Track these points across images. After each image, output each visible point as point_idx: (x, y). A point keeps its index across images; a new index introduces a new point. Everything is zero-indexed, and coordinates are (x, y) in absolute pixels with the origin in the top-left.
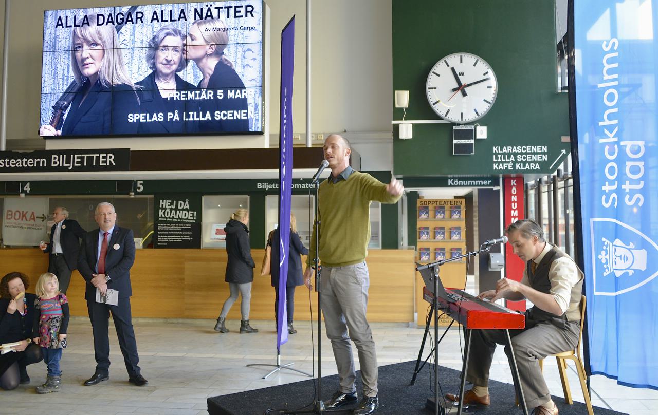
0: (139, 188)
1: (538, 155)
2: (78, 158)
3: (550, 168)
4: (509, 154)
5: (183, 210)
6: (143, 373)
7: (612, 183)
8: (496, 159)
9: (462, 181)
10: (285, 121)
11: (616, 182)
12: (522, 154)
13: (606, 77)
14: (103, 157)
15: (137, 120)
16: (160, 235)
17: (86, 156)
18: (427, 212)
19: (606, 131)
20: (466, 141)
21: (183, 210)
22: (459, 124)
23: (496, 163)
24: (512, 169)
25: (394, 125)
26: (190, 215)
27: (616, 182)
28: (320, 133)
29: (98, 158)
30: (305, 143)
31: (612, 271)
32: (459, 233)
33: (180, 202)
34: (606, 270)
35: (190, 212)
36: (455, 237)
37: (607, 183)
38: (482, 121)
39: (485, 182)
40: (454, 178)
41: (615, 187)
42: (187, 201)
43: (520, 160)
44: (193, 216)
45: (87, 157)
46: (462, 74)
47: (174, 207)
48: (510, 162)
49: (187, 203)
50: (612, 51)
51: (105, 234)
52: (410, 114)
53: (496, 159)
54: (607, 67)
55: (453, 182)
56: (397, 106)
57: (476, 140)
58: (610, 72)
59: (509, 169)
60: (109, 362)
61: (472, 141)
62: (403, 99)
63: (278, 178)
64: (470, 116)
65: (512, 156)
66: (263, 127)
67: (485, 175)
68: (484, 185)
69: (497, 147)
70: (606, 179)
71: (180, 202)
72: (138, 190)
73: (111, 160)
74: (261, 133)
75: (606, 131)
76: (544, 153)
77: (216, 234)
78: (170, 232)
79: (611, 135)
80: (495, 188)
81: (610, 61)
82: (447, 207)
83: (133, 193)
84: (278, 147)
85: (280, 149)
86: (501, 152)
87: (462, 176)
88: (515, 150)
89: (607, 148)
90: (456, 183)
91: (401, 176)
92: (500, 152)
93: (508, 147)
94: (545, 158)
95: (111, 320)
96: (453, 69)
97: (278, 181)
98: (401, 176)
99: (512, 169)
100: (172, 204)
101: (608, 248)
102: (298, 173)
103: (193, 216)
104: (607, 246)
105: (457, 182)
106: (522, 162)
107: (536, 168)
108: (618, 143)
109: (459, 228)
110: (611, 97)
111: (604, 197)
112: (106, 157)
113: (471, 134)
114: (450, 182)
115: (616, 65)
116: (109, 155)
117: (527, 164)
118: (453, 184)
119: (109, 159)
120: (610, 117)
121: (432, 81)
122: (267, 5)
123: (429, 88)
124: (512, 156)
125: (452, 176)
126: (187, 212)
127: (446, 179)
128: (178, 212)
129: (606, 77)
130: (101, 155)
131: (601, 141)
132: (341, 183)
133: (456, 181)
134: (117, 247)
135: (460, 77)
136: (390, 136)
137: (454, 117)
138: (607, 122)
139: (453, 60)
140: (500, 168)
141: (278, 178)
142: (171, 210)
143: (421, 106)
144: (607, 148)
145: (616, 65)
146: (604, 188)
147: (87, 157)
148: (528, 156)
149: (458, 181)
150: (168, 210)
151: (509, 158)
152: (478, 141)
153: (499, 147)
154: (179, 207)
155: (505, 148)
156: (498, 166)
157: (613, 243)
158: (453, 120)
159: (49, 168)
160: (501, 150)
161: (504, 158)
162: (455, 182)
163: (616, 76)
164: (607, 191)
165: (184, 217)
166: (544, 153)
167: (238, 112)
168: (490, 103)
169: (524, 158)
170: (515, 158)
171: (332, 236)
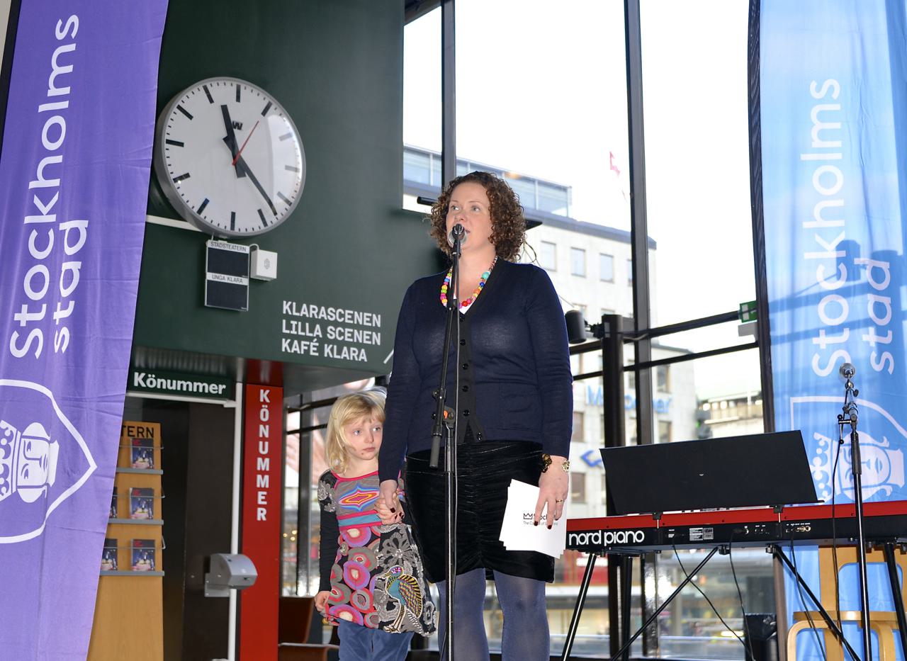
1: (365, 332)
3: (385, 362)
4: (313, 322)
7: (34, 306)
8: (286, 329)
9: (163, 381)
11: (44, 306)
12: (336, 324)
13: (53, 91)
15: (305, 350)
19: (37, 201)
20: (233, 277)
23: (287, 336)
24: (317, 354)
27: (44, 306)
31: (14, 490)
37: (25, 307)
38: (263, 240)
41: (39, 316)
48: (313, 338)
50: (67, 40)
53: (286, 329)
54: (57, 70)
55: (145, 380)
57: (251, 280)
59: (312, 353)
61: (245, 281)
64: (249, 224)
65: (318, 327)
69: (290, 303)
70: (25, 299)
75: (37, 201)
76: (375, 329)
86: (298, 314)
88: (323, 315)
89: (34, 234)
90: (151, 383)
92: (295, 314)
93: (312, 306)
94: (377, 339)
96: (225, 109)
99: (317, 354)
101: (12, 444)
104: (10, 439)
106: (335, 341)
107: (361, 358)
108: (54, 225)
110: (54, 133)
111: (15, 335)
113: (240, 264)
117: (345, 349)
118: (143, 385)
120: (49, 172)
124: (318, 327)
129: (53, 91)
133: (151, 378)
137: (216, 217)
138: (41, 183)
140: (294, 349)
144: (34, 234)
146: (17, 317)
148: (347, 330)
149: (156, 379)
151: (312, 330)
152: (256, 282)
153: (294, 304)
155: (305, 306)
156: (291, 345)
157: (22, 432)
160: (298, 310)
161: (303, 330)
162: (148, 381)
163: (66, 91)
164: (23, 324)
166: (375, 329)
169: (341, 334)
170: (324, 331)
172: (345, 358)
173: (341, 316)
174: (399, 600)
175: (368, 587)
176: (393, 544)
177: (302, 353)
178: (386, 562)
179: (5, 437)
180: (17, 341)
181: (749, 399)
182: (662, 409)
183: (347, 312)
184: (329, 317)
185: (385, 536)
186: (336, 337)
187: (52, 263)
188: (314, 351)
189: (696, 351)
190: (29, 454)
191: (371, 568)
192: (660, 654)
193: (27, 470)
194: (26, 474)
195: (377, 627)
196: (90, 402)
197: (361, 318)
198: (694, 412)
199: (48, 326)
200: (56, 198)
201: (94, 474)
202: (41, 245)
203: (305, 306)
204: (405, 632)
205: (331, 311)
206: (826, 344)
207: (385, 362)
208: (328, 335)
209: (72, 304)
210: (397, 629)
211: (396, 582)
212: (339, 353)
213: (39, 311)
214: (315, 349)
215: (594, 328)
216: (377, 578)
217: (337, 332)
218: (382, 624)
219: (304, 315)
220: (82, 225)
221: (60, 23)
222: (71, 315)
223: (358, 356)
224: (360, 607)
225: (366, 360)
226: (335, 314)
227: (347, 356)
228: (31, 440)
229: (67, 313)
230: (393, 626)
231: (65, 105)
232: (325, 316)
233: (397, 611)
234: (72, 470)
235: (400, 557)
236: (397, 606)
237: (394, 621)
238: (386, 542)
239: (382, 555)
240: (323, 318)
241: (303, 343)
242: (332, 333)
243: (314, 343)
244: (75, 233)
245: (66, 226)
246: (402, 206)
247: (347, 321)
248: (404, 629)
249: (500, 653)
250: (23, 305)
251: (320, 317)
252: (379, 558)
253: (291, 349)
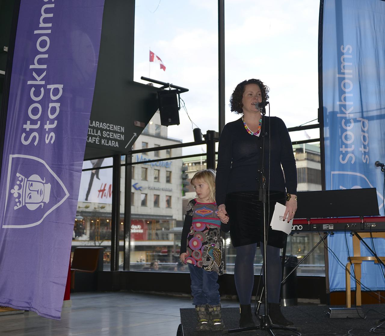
1: (118, 134)
3: (126, 148)
4: (97, 129)
7: (34, 122)
11: (39, 122)
12: (106, 130)
13: (42, 25)
15: (94, 141)
19: (34, 74)
24: (99, 143)
27: (39, 122)
31: (24, 204)
34: (18, 204)
37: (29, 122)
41: (37, 127)
43: (105, 136)
48: (97, 136)
54: (44, 15)
58: (46, 21)
59: (97, 143)
65: (99, 131)
70: (28, 118)
75: (34, 74)
79: (39, 79)
81: (47, 11)
89: (33, 89)
93: (97, 122)
94: (123, 137)
101: (22, 184)
104: (21, 181)
106: (106, 138)
107: (116, 145)
108: (44, 86)
115: (51, 15)
120: (40, 62)
124: (99, 131)
131: (29, 82)
138: (36, 66)
144: (33, 89)
145: (51, 15)
146: (25, 126)
148: (111, 133)
151: (97, 133)
155: (94, 122)
161: (93, 132)
163: (50, 25)
164: (28, 130)
167: (116, 126)
170: (102, 133)
172: (110, 145)
173: (109, 127)
174: (212, 258)
175: (200, 249)
176: (214, 234)
177: (93, 142)
178: (210, 240)
179: (19, 180)
180: (342, 158)
181: (201, 163)
182: (167, 166)
183: (111, 125)
184: (104, 127)
185: (211, 230)
186: (106, 136)
187: (45, 102)
188: (97, 142)
189: (184, 142)
190: (31, 188)
191: (203, 242)
192: (226, 272)
193: (31, 195)
194: (30, 197)
195: (202, 267)
196: (65, 166)
197: (117, 128)
198: (181, 167)
199: (41, 131)
200: (45, 74)
201: (68, 198)
202: (37, 94)
203: (94, 122)
204: (213, 271)
205: (105, 125)
206: (30, 129)
207: (126, 148)
208: (103, 135)
209: (56, 122)
210: (209, 269)
211: (212, 249)
212: (108, 143)
213: (36, 124)
214: (98, 141)
215: (204, 136)
216: (205, 246)
217: (107, 134)
218: (204, 266)
219: (94, 126)
220: (60, 87)
222: (56, 126)
223: (115, 145)
224: (196, 258)
225: (118, 147)
226: (106, 126)
227: (111, 144)
228: (33, 182)
229: (53, 126)
230: (208, 268)
231: (49, 31)
232: (102, 126)
233: (211, 262)
234: (57, 196)
235: (216, 240)
236: (211, 260)
237: (208, 266)
238: (211, 232)
239: (208, 237)
240: (101, 127)
241: (93, 138)
242: (105, 134)
243: (98, 139)
244: (56, 91)
245: (52, 87)
246: (133, 80)
247: (111, 129)
248: (212, 270)
249: (190, 273)
250: (28, 121)
251: (100, 127)
252: (207, 238)
253: (88, 141)
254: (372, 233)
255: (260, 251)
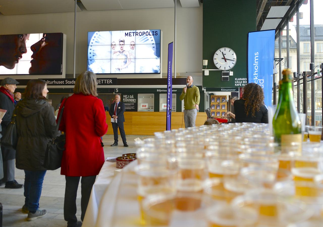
0: (117, 91)
2: (100, 81)
4: (240, 81)
5: (131, 98)
6: (128, 144)
10: (169, 71)
12: (244, 81)
13: (255, 62)
14: (108, 81)
16: (125, 107)
17: (102, 80)
18: (214, 100)
19: (255, 77)
21: (131, 98)
22: (224, 71)
23: (236, 83)
25: (203, 71)
26: (134, 100)
28: (178, 73)
29: (106, 81)
30: (174, 76)
32: (225, 107)
33: (130, 96)
35: (134, 99)
36: (223, 108)
38: (231, 70)
39: (234, 90)
40: (223, 89)
42: (133, 95)
44: (135, 101)
45: (103, 81)
46: (225, 54)
47: (128, 97)
49: (133, 96)
50: (257, 55)
51: (116, 104)
52: (208, 67)
54: (256, 60)
55: (223, 90)
56: (204, 65)
58: (256, 61)
60: (118, 141)
61: (228, 76)
62: (206, 62)
63: (167, 88)
64: (228, 68)
65: (241, 81)
66: (160, 72)
67: (234, 88)
68: (233, 91)
71: (130, 96)
72: (116, 92)
73: (111, 81)
74: (160, 73)
75: (255, 77)
77: (146, 105)
78: (127, 106)
80: (237, 92)
81: (256, 58)
82: (221, 98)
83: (114, 93)
84: (167, 78)
85: (167, 79)
87: (226, 88)
88: (242, 79)
89: (255, 81)
91: (205, 88)
92: (237, 80)
95: (118, 129)
96: (222, 53)
97: (167, 89)
98: (205, 88)
100: (128, 96)
102: (174, 86)
103: (135, 101)
105: (224, 90)
108: (258, 80)
109: (225, 105)
112: (109, 81)
113: (228, 74)
114: (222, 90)
115: (258, 59)
116: (110, 80)
119: (110, 81)
120: (256, 73)
121: (215, 56)
122: (161, 31)
123: (214, 59)
124: (241, 81)
125: (222, 88)
126: (132, 99)
127: (221, 89)
128: (130, 99)
129: (255, 62)
130: (108, 80)
132: (191, 88)
134: (119, 108)
135: (225, 55)
136: (202, 74)
138: (255, 74)
139: (222, 50)
141: (167, 88)
142: (127, 98)
143: (212, 65)
144: (255, 81)
145: (258, 59)
147: (103, 81)
150: (126, 99)
151: (240, 82)
152: (230, 76)
154: (130, 98)
155: (239, 79)
158: (222, 69)
159: (65, 84)
160: (238, 79)
161: (239, 82)
163: (258, 62)
165: (132, 101)
168: (234, 64)
170: (242, 82)
171: (82, 218)
203: (239, 79)
221: (255, 53)
231: (258, 64)
243: (241, 84)
254: (311, 81)
255: (308, 96)
